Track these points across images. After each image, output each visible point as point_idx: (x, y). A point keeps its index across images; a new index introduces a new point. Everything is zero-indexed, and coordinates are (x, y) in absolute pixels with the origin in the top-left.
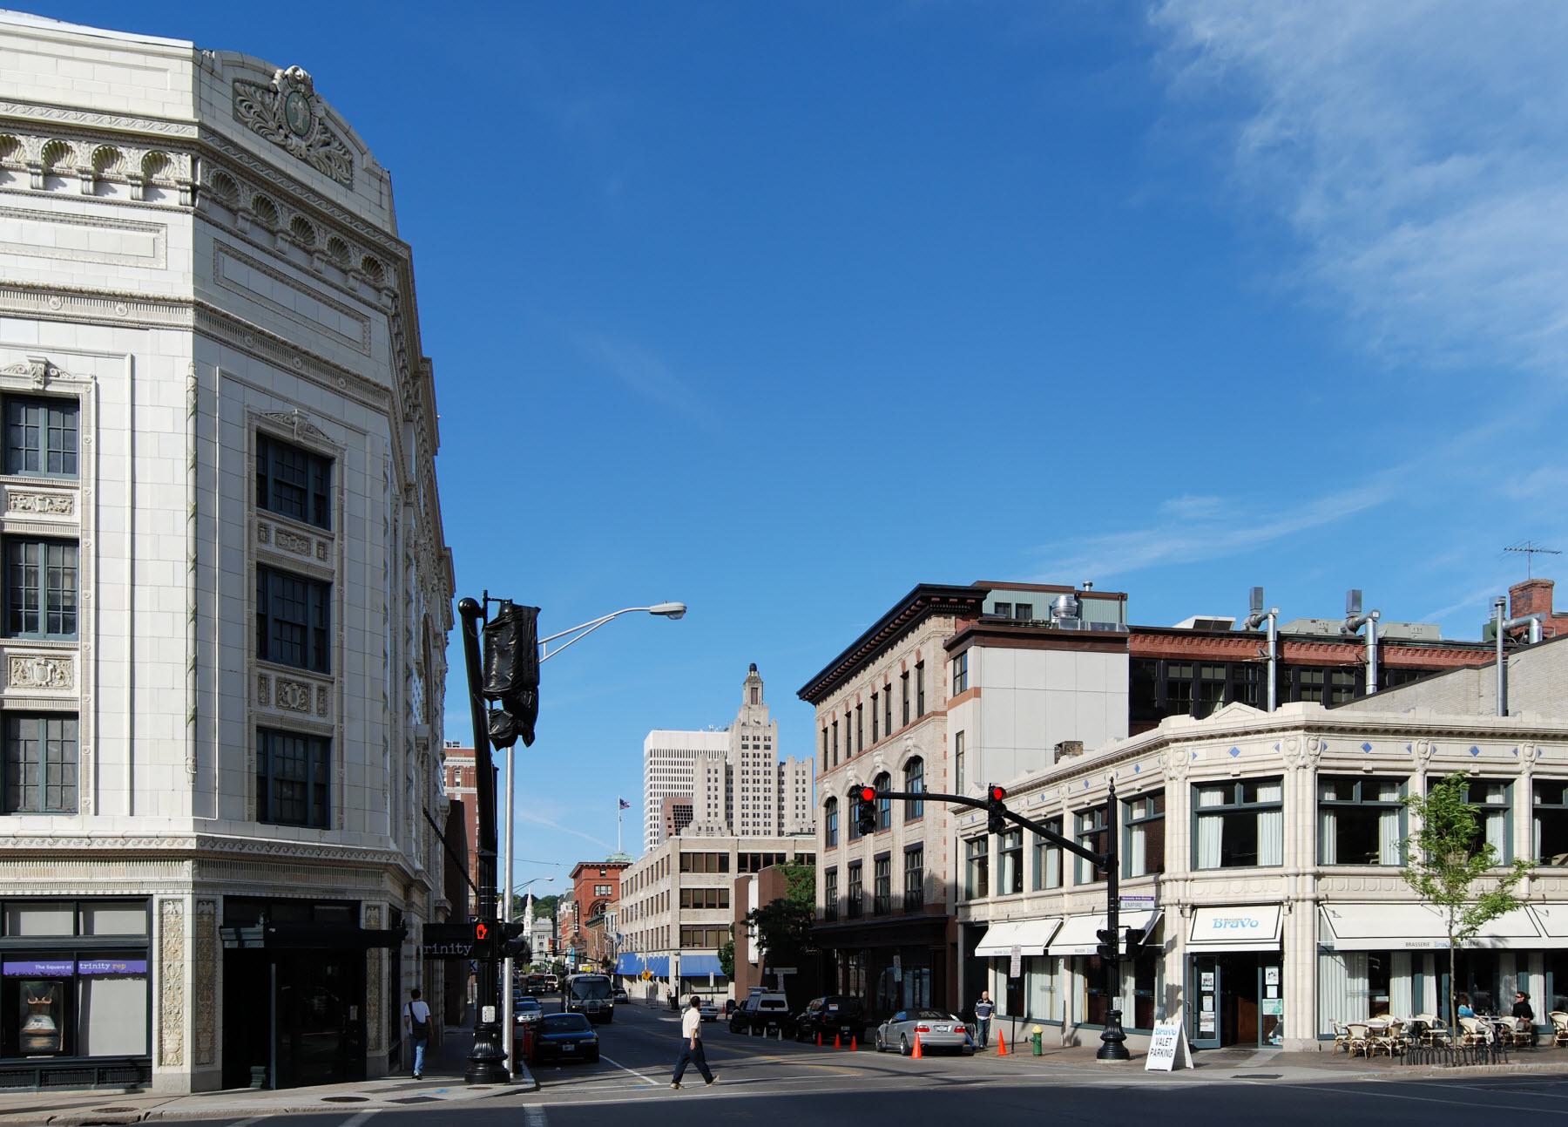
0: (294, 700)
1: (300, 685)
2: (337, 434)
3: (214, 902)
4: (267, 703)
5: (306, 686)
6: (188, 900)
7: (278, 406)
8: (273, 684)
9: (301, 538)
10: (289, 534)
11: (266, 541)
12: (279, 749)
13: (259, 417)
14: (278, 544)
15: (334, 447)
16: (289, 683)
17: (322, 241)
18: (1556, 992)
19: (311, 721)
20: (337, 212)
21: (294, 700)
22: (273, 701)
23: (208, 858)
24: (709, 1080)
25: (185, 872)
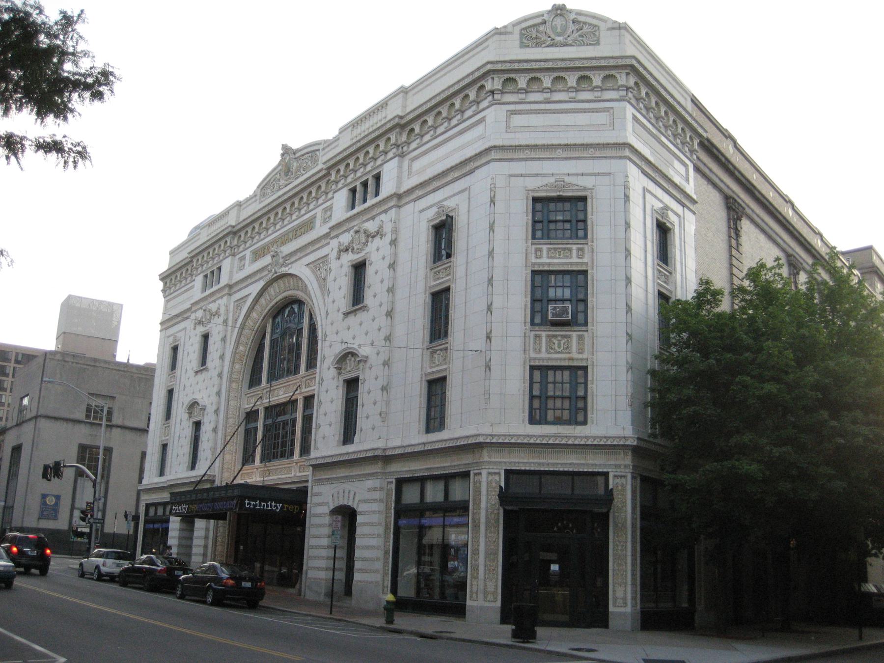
0: (559, 347)
1: (564, 337)
2: (587, 182)
3: (625, 477)
4: (540, 351)
5: (569, 337)
6: (629, 476)
7: (551, 180)
8: (544, 340)
9: (564, 249)
10: (555, 249)
11: (541, 257)
12: (551, 379)
13: (533, 191)
14: (548, 257)
15: (585, 189)
16: (555, 336)
17: (597, 80)
18: (23, 355)
19: (574, 355)
20: (509, 65)
21: (559, 347)
22: (544, 349)
23: (638, 452)
24: (97, 567)
25: (627, 460)
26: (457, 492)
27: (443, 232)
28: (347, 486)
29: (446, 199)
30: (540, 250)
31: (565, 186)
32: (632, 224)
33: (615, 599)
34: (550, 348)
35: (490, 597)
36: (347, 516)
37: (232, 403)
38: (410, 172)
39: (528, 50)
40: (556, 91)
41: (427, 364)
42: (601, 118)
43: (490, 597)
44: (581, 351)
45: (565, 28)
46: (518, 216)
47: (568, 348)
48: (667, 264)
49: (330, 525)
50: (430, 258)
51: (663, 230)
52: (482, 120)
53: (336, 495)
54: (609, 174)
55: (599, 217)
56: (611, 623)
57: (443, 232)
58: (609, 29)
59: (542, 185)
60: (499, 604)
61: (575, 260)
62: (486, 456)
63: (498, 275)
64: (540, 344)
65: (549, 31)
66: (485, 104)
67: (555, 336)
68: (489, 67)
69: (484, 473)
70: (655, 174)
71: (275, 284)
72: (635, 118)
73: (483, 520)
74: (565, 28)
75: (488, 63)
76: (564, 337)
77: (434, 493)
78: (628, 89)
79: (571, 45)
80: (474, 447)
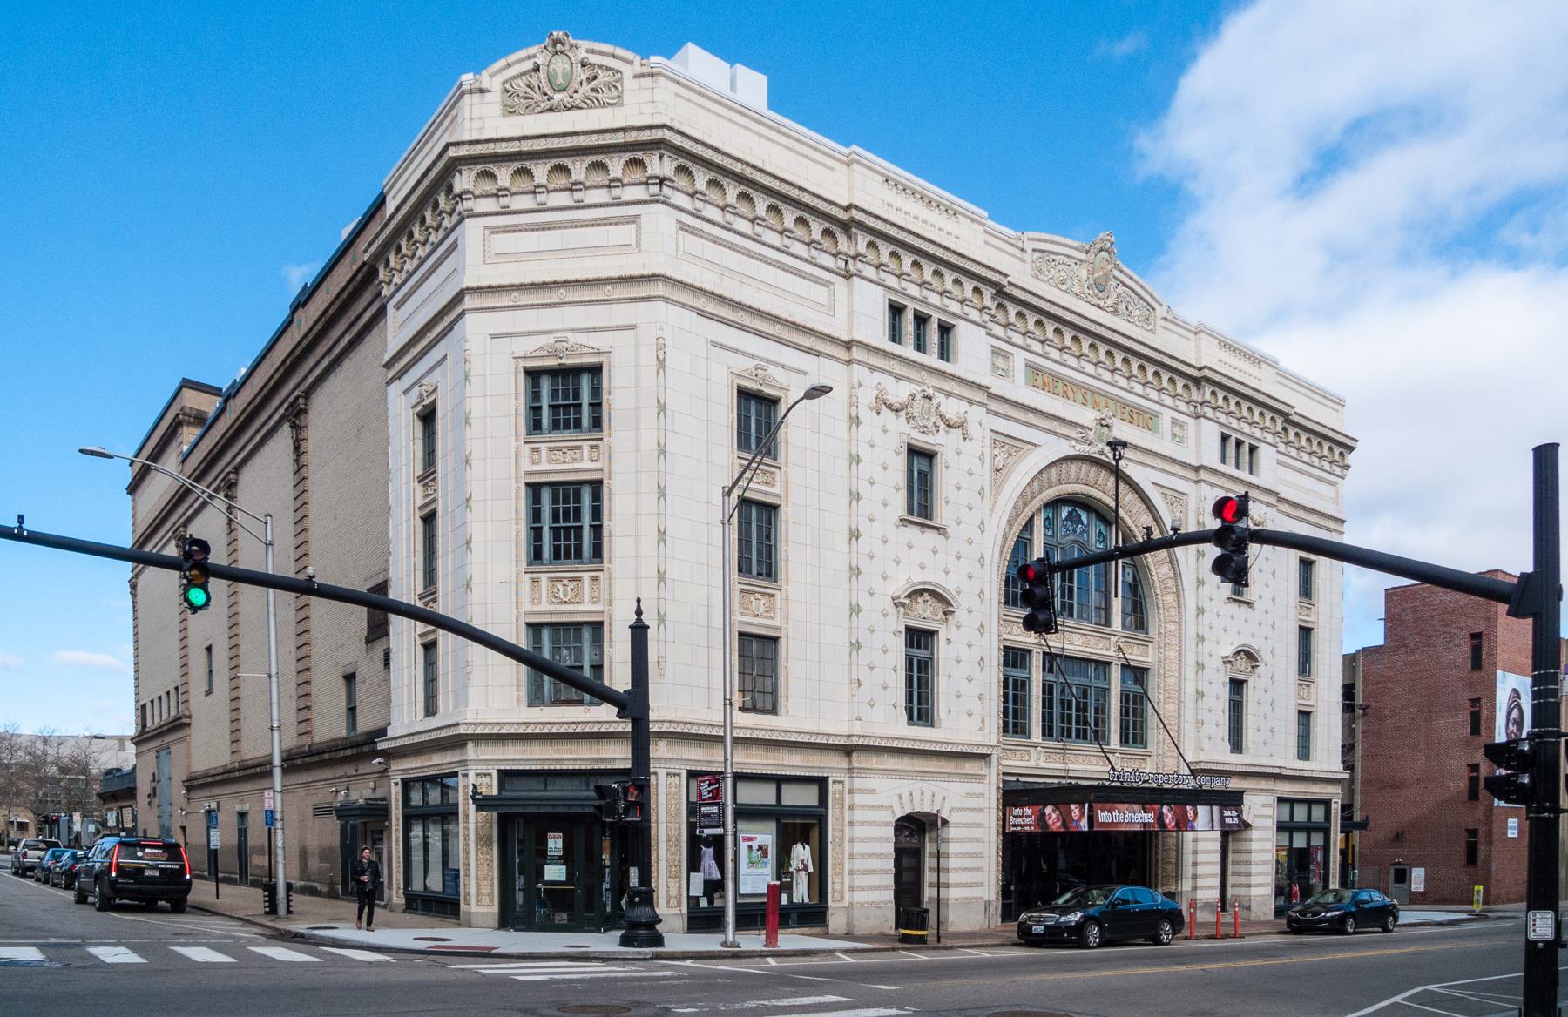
1: (572, 580)
7: (550, 339)
16: (560, 580)
28: (930, 786)
30: (537, 450)
35: (485, 900)
36: (916, 831)
37: (1172, 654)
39: (515, 119)
40: (555, 190)
42: (623, 233)
44: (595, 600)
45: (569, 78)
47: (578, 595)
49: (946, 840)
53: (906, 797)
54: (633, 327)
58: (635, 77)
59: (537, 349)
61: (587, 464)
62: (471, 751)
64: (539, 589)
65: (545, 86)
67: (560, 580)
69: (472, 774)
71: (1085, 467)
74: (569, 78)
75: (663, 126)
76: (572, 580)
78: (662, 181)
79: (579, 108)
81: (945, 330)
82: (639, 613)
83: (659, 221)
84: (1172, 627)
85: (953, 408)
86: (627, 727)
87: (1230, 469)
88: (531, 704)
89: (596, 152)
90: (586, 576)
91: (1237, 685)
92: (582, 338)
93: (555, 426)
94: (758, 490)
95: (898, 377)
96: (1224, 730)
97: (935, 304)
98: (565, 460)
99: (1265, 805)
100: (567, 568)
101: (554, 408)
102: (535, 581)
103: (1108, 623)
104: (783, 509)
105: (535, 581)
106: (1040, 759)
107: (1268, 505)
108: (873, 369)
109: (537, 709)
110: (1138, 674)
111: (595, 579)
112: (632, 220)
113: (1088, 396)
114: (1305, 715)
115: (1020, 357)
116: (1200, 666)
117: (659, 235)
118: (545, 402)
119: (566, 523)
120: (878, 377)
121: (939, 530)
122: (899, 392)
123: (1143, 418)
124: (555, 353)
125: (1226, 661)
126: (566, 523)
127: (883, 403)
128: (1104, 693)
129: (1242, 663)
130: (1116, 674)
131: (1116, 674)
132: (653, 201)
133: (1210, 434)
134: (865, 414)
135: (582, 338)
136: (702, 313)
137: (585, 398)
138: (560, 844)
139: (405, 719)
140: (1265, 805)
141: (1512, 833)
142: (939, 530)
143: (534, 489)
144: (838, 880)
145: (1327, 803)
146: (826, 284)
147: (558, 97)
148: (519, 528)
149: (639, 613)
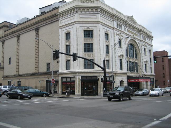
2: (93, 28)
7: (87, 27)
11: (86, 57)
15: (93, 29)
26: (72, 79)
27: (68, 35)
29: (69, 29)
30: (85, 39)
31: (89, 29)
32: (101, 49)
33: (99, 91)
34: (87, 56)
35: (79, 92)
37: (140, 61)
38: (61, 23)
41: (66, 58)
42: (95, 17)
43: (79, 92)
46: (82, 34)
47: (90, 56)
48: (108, 40)
50: (65, 39)
51: (107, 35)
52: (74, 16)
55: (95, 33)
56: (98, 94)
57: (68, 35)
59: (85, 28)
60: (81, 93)
61: (91, 57)
63: (78, 39)
66: (75, 13)
68: (76, 7)
70: (104, 25)
72: (101, 16)
73: (78, 85)
75: (100, 6)
77: (69, 80)
78: (99, 12)
80: (75, 73)
81: (121, 26)
82: (104, 59)
83: (99, 16)
84: (140, 58)
85: (122, 34)
86: (103, 71)
87: (118, 28)
88: (85, 68)
89: (92, 8)
90: (91, 54)
91: (146, 65)
92: (90, 27)
93: (87, 37)
94: (108, 44)
95: (118, 31)
96: (119, 67)
97: (120, 24)
98: (89, 41)
99: (126, 78)
100: (89, 53)
101: (87, 35)
102: (85, 54)
103: (134, 57)
104: (109, 46)
105: (85, 54)
106: (130, 74)
107: (123, 34)
108: (116, 31)
109: (86, 69)
110: (137, 63)
111: (92, 54)
112: (96, 15)
113: (132, 33)
114: (151, 68)
115: (126, 28)
116: (115, 57)
117: (99, 18)
118: (86, 34)
119: (89, 48)
120: (116, 31)
121: (122, 48)
122: (118, 33)
123: (136, 35)
124: (87, 29)
125: (119, 56)
126: (89, 48)
127: (117, 34)
128: (134, 66)
129: (121, 57)
130: (135, 63)
131: (135, 63)
132: (98, 13)
133: (115, 23)
134: (115, 35)
135: (90, 27)
136: (103, 25)
137: (91, 34)
138: (89, 86)
139: (62, 69)
140: (126, 78)
141: (168, 82)
142: (122, 48)
143: (85, 44)
144: (100, 90)
145: (153, 78)
146: (111, 21)
147: (87, 2)
148: (106, 52)
149: (104, 59)
